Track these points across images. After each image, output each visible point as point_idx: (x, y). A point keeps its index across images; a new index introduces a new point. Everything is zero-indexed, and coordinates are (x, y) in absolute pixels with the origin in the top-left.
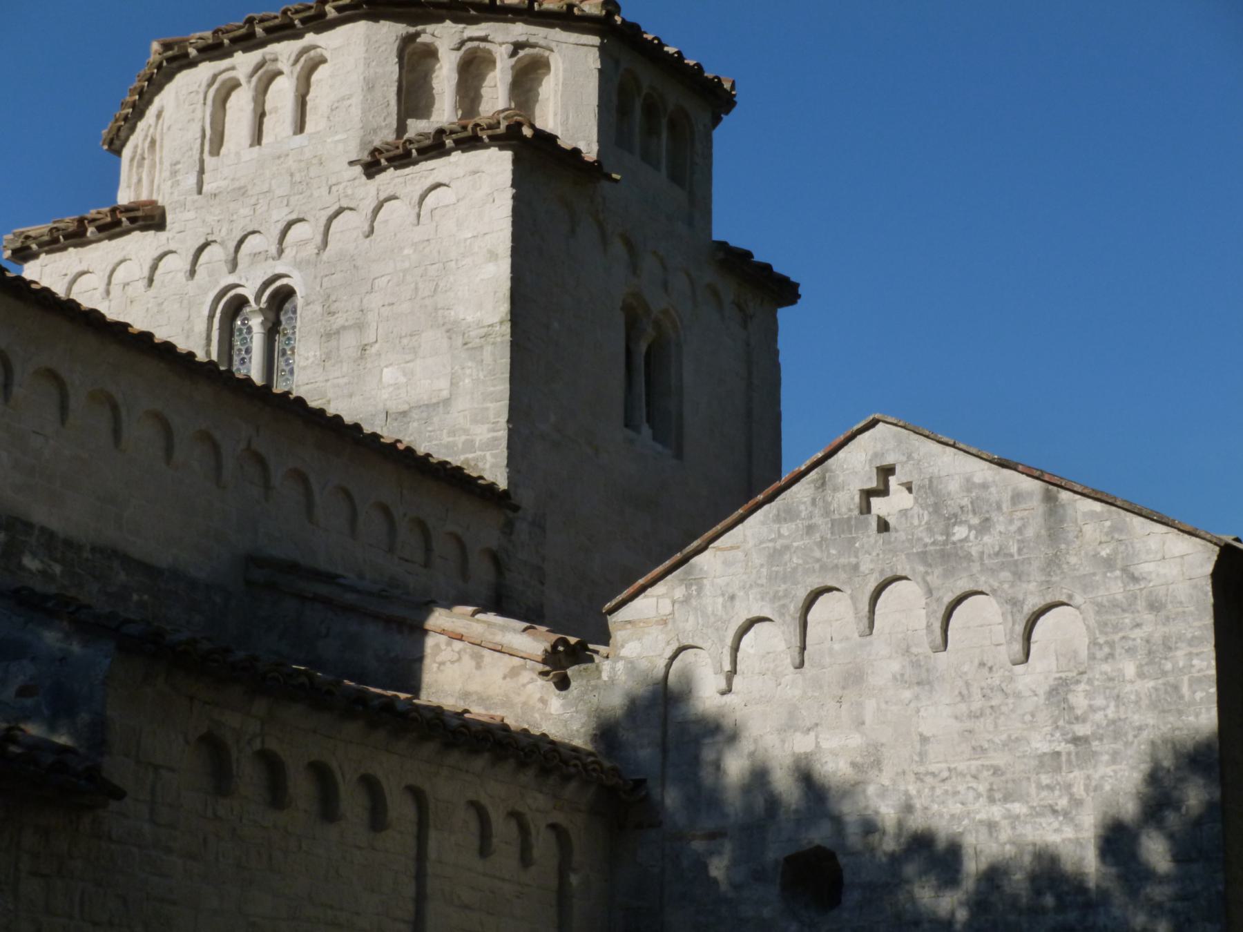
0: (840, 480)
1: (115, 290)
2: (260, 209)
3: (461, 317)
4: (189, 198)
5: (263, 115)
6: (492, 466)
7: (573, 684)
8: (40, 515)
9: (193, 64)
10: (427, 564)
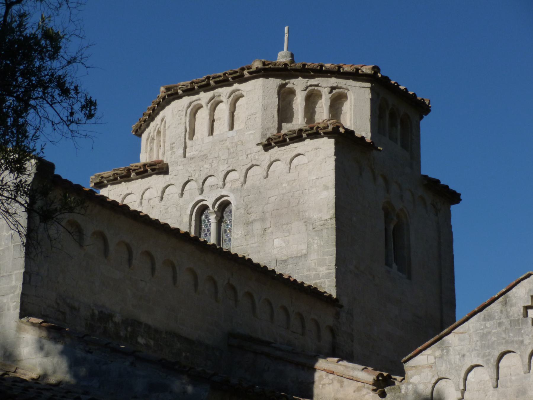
0: (514, 301)
1: (145, 202)
2: (215, 164)
3: (312, 216)
4: (180, 160)
5: (213, 121)
6: (329, 286)
7: (388, 395)
8: (144, 318)
9: (180, 97)
10: (303, 334)
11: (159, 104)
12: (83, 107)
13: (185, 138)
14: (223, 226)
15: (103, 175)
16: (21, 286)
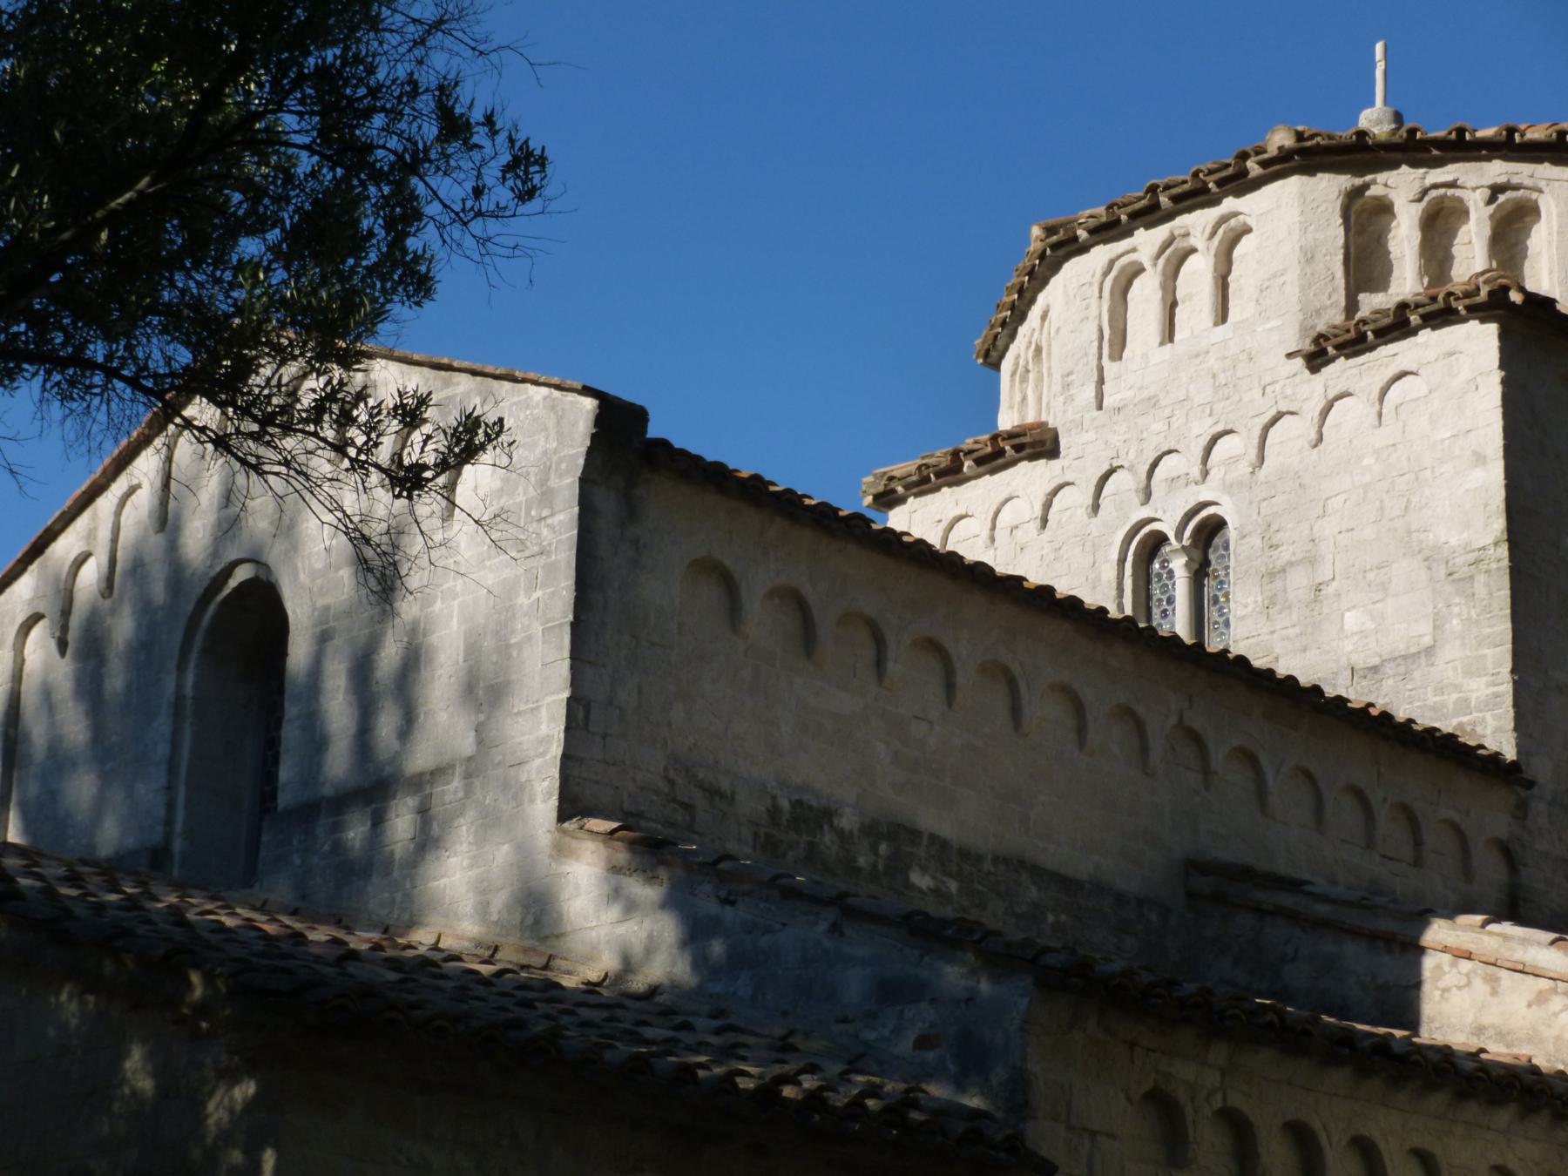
2: (1178, 421)
3: (1443, 540)
5: (1174, 304)
6: (1497, 730)
8: (929, 820)
9: (1084, 249)
10: (1417, 863)
11: (1031, 273)
12: (508, 168)
13: (1100, 357)
14: (1209, 586)
15: (896, 473)
16: (562, 736)
